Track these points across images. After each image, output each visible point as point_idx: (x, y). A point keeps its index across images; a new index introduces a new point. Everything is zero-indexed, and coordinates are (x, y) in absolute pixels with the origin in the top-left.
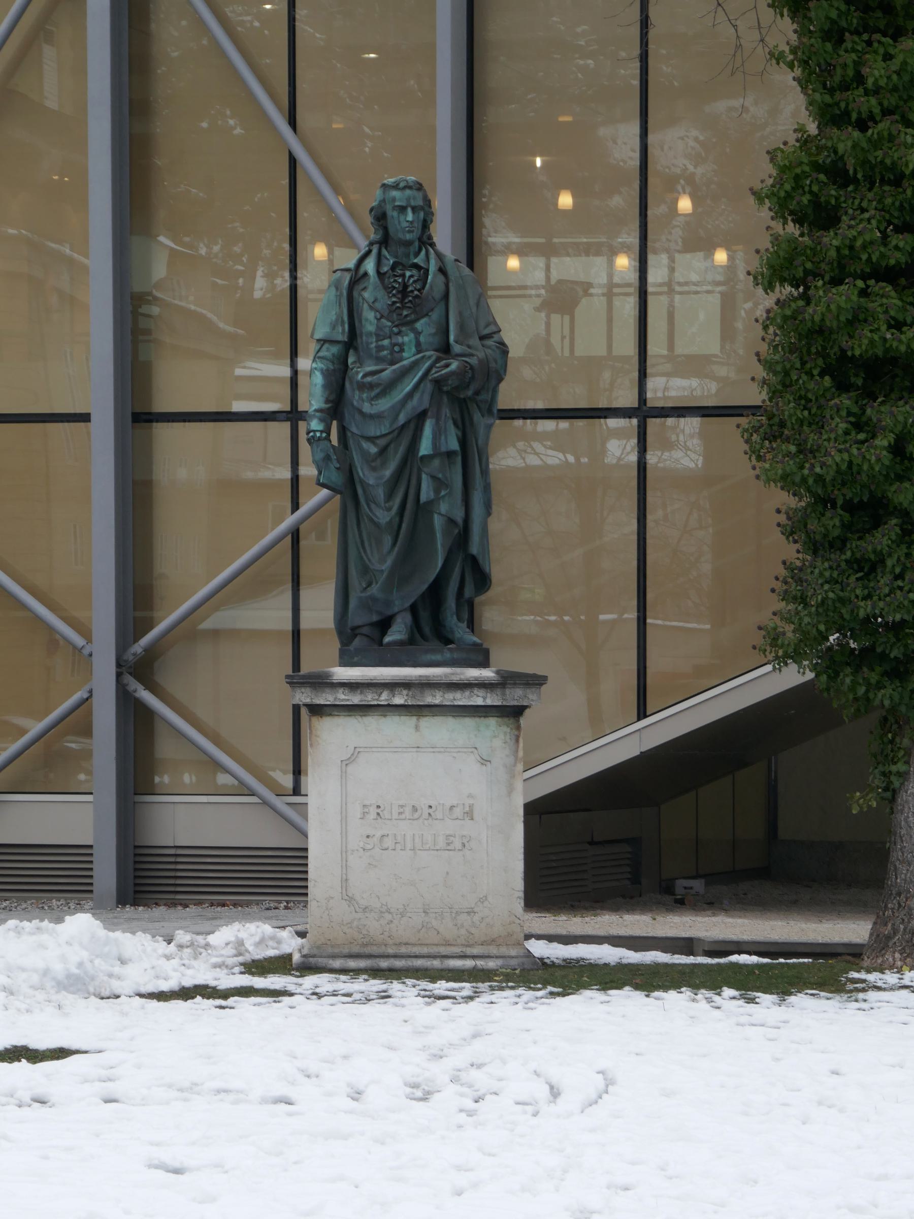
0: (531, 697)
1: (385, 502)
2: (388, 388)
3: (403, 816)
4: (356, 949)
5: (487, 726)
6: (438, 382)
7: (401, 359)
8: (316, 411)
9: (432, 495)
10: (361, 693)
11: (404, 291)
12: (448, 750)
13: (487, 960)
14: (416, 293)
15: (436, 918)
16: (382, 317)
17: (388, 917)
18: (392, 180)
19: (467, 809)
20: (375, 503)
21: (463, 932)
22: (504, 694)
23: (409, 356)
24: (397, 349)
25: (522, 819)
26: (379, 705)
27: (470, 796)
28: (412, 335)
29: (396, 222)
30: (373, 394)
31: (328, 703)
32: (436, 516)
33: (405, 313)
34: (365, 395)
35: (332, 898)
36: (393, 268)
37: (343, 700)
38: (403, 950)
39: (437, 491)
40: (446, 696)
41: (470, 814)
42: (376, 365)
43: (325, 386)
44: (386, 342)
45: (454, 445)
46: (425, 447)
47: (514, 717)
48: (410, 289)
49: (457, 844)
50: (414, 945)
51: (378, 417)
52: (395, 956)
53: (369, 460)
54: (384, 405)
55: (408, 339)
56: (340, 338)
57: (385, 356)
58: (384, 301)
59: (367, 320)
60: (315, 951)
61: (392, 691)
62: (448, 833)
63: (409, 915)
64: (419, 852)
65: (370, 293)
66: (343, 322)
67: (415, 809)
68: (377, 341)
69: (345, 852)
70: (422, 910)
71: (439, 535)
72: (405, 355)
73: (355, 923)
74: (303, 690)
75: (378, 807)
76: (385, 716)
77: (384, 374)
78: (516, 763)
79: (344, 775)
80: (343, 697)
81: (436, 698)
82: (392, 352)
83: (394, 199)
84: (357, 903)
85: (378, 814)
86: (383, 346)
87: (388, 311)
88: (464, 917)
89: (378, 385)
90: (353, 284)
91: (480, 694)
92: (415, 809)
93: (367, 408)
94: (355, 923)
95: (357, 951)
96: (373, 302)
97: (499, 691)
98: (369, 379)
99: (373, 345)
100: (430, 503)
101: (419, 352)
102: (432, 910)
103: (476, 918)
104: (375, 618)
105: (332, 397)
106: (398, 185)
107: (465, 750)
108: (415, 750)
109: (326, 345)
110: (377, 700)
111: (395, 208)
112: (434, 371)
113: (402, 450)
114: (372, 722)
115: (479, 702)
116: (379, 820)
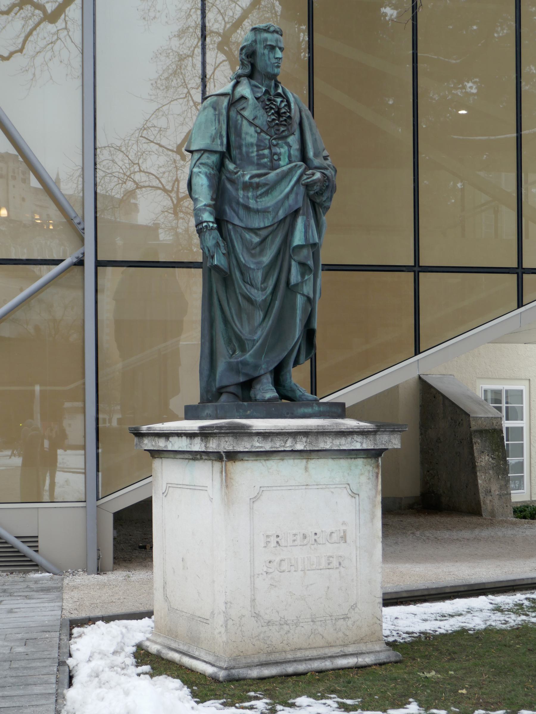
0: (394, 441)
1: (262, 283)
2: (271, 188)
3: (296, 543)
4: (263, 658)
5: (356, 466)
6: (307, 186)
7: (279, 167)
8: (205, 205)
10: (271, 441)
11: (278, 114)
12: (328, 486)
13: (364, 656)
15: (321, 626)
17: (286, 628)
18: (264, 25)
19: (342, 534)
20: (252, 285)
21: (341, 635)
22: (375, 440)
23: (284, 165)
24: (276, 157)
25: (381, 540)
26: (284, 451)
27: (344, 523)
28: (286, 148)
29: (267, 58)
30: (259, 193)
31: (247, 450)
32: (299, 296)
33: (282, 129)
34: (250, 194)
35: (244, 616)
37: (258, 447)
38: (299, 655)
39: (303, 275)
40: (334, 442)
41: (344, 538)
42: (258, 169)
43: (210, 186)
44: (266, 152)
46: (298, 239)
47: (375, 458)
49: (335, 563)
50: (306, 649)
51: (264, 211)
52: (295, 661)
53: (249, 248)
54: (268, 202)
55: (283, 150)
56: (219, 149)
57: (266, 163)
58: (263, 119)
59: (247, 133)
60: (233, 663)
61: (294, 438)
62: (328, 554)
63: (301, 624)
64: (308, 572)
66: (221, 136)
67: (305, 537)
68: (257, 151)
69: (253, 576)
70: (310, 620)
71: (299, 312)
72: (282, 163)
73: (262, 636)
74: (227, 439)
75: (278, 536)
76: (283, 460)
78: (376, 494)
79: (251, 508)
80: (258, 444)
81: (327, 444)
83: (266, 40)
84: (263, 619)
85: (277, 542)
86: (264, 155)
87: (267, 127)
88: (341, 622)
89: (265, 185)
90: (232, 104)
91: (359, 440)
92: (305, 537)
93: (252, 204)
94: (262, 636)
95: (264, 659)
96: (253, 119)
97: (371, 437)
98: (257, 180)
99: (255, 154)
100: (297, 285)
101: (290, 162)
102: (318, 619)
103: (350, 623)
104: (242, 379)
106: (269, 28)
108: (304, 487)
110: (284, 446)
112: (305, 177)
113: (278, 241)
114: (273, 464)
115: (358, 446)
116: (278, 548)
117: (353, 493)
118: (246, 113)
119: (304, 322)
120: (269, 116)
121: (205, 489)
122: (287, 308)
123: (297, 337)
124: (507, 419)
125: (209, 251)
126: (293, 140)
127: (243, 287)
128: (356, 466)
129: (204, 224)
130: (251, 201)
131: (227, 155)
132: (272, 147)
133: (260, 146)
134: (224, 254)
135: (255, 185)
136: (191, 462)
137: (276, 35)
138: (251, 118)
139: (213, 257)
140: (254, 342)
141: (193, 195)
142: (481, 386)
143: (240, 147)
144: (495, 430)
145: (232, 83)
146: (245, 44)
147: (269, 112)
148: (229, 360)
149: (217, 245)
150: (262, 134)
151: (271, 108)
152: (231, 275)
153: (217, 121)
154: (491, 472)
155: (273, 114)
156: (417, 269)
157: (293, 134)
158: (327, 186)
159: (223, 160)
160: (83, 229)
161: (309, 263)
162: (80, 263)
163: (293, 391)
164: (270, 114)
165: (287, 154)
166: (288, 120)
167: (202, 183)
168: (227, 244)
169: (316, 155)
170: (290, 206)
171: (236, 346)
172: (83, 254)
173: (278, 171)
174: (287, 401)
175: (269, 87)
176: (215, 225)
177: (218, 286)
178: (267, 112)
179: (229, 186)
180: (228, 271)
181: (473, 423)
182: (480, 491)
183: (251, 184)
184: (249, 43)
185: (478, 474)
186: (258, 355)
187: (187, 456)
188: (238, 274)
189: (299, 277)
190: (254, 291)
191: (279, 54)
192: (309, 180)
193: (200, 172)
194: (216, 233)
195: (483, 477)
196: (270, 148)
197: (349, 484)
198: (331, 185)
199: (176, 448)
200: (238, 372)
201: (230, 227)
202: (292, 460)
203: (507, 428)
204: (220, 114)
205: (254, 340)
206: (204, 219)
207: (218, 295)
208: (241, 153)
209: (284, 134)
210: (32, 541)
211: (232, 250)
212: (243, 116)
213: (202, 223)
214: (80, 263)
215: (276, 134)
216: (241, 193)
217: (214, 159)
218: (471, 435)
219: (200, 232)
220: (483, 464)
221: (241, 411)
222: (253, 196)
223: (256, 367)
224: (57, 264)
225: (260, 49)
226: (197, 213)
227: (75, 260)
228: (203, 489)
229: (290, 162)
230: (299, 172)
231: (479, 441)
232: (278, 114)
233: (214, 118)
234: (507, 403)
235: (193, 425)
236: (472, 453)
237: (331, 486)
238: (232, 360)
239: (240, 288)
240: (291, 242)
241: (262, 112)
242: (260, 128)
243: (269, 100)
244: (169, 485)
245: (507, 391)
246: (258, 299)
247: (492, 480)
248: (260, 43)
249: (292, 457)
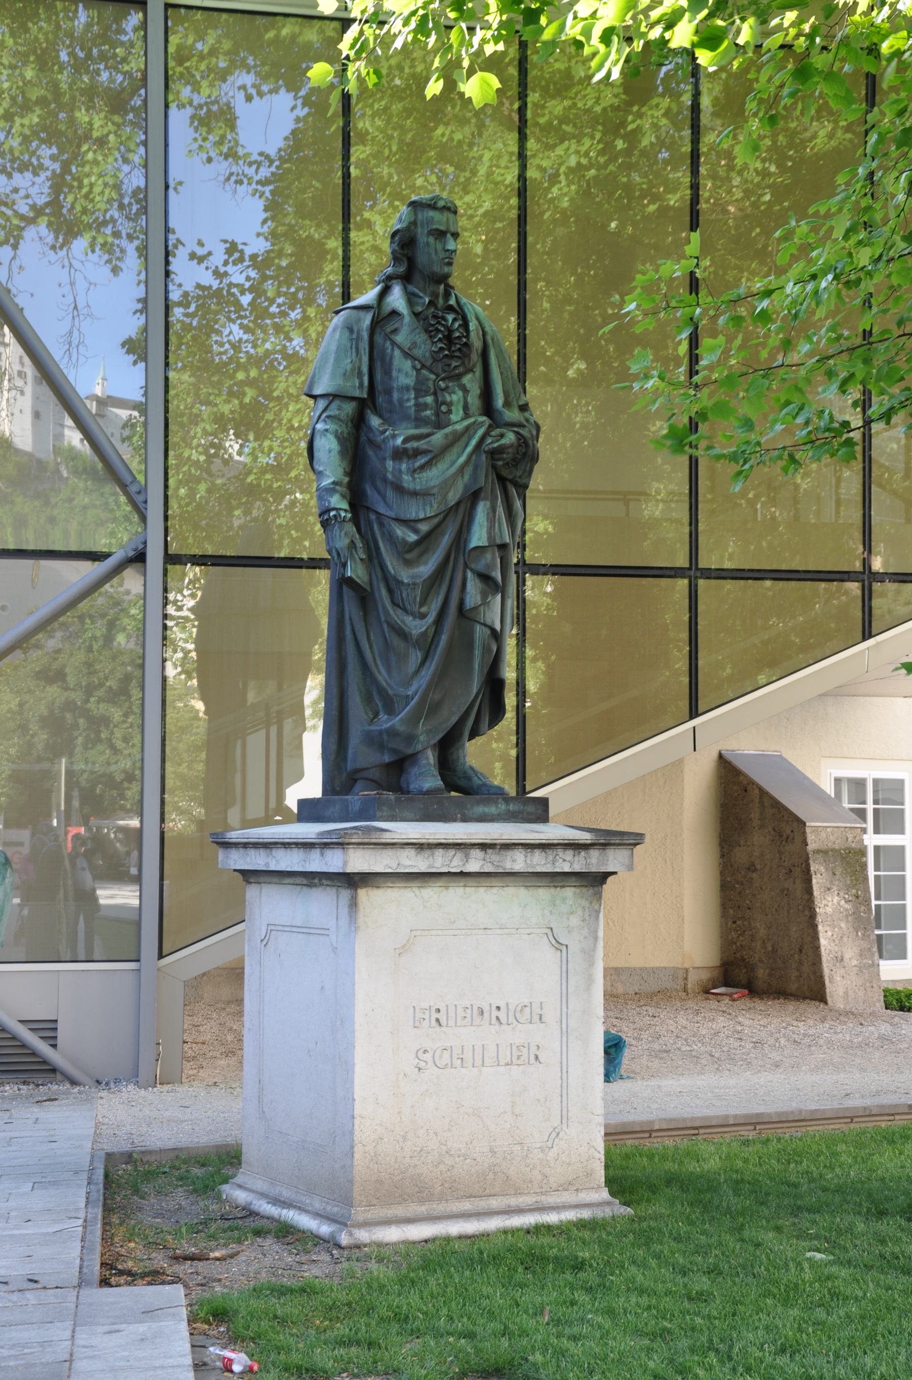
2: (435, 457)
6: (493, 454)
9: (479, 600)
11: (449, 338)
20: (405, 610)
24: (444, 408)
28: (460, 394)
29: (432, 251)
30: (418, 464)
32: (478, 627)
33: (454, 364)
34: (404, 466)
39: (484, 595)
42: (416, 427)
43: (343, 453)
44: (429, 399)
46: (478, 537)
48: (457, 334)
54: (433, 476)
56: (357, 393)
58: (424, 347)
59: (399, 371)
65: (406, 333)
66: (360, 374)
68: (416, 398)
76: (447, 887)
77: (433, 438)
81: (518, 862)
82: (438, 413)
83: (431, 220)
89: (426, 452)
98: (414, 444)
99: (412, 402)
100: (475, 609)
104: (387, 758)
108: (481, 932)
109: (337, 403)
111: (432, 232)
112: (489, 440)
113: (446, 540)
114: (431, 893)
118: (399, 338)
119: (486, 671)
120: (433, 343)
121: (327, 932)
122: (463, 643)
123: (475, 691)
124: (877, 831)
125: (339, 554)
126: (472, 381)
127: (392, 612)
129: (332, 513)
130: (405, 477)
131: (370, 404)
132: (439, 393)
133: (420, 389)
134: (361, 560)
135: (411, 453)
136: (305, 888)
137: (446, 214)
138: (406, 345)
139: (344, 565)
140: (408, 699)
141: (316, 467)
142: (829, 771)
143: (388, 392)
144: (849, 851)
145: (378, 288)
146: (398, 227)
147: (435, 337)
148: (367, 728)
149: (352, 544)
150: (424, 372)
151: (438, 330)
152: (372, 593)
154: (843, 925)
155: (440, 340)
156: (694, 572)
157: (472, 371)
158: (525, 455)
159: (360, 414)
160: (146, 502)
161: (493, 574)
162: (139, 558)
163: (469, 778)
165: (462, 403)
166: (464, 349)
167: (328, 447)
168: (368, 544)
169: (507, 404)
171: (380, 704)
172: (145, 543)
174: (461, 791)
175: (435, 295)
176: (349, 515)
177: (352, 609)
178: (431, 337)
179: (370, 452)
180: (368, 589)
181: (810, 837)
182: (824, 959)
183: (405, 451)
184: (405, 225)
185: (820, 928)
186: (414, 719)
187: (299, 880)
188: (384, 592)
189: (479, 598)
190: (409, 619)
191: (451, 245)
192: (495, 445)
193: (326, 430)
194: (351, 528)
195: (830, 933)
196: (435, 394)
198: (530, 452)
199: (282, 867)
200: (382, 747)
201: (373, 517)
203: (877, 849)
204: (359, 339)
205: (407, 696)
206: (332, 505)
207: (352, 624)
208: (390, 402)
210: (48, 1029)
211: (374, 554)
212: (394, 343)
213: (329, 510)
215: (445, 371)
216: (390, 464)
217: (349, 408)
218: (807, 859)
219: (325, 524)
220: (829, 910)
221: (385, 808)
222: (408, 469)
223: (410, 739)
225: (422, 237)
226: (323, 493)
227: (131, 554)
228: (322, 932)
229: (467, 415)
230: (480, 432)
231: (822, 869)
232: (449, 338)
234: (876, 802)
235: (310, 830)
236: (809, 891)
238: (373, 728)
239: (387, 613)
240: (466, 542)
241: (424, 336)
242: (420, 362)
243: (435, 317)
244: (270, 927)
245: (876, 782)
246: (414, 632)
247: (845, 939)
248: (422, 227)
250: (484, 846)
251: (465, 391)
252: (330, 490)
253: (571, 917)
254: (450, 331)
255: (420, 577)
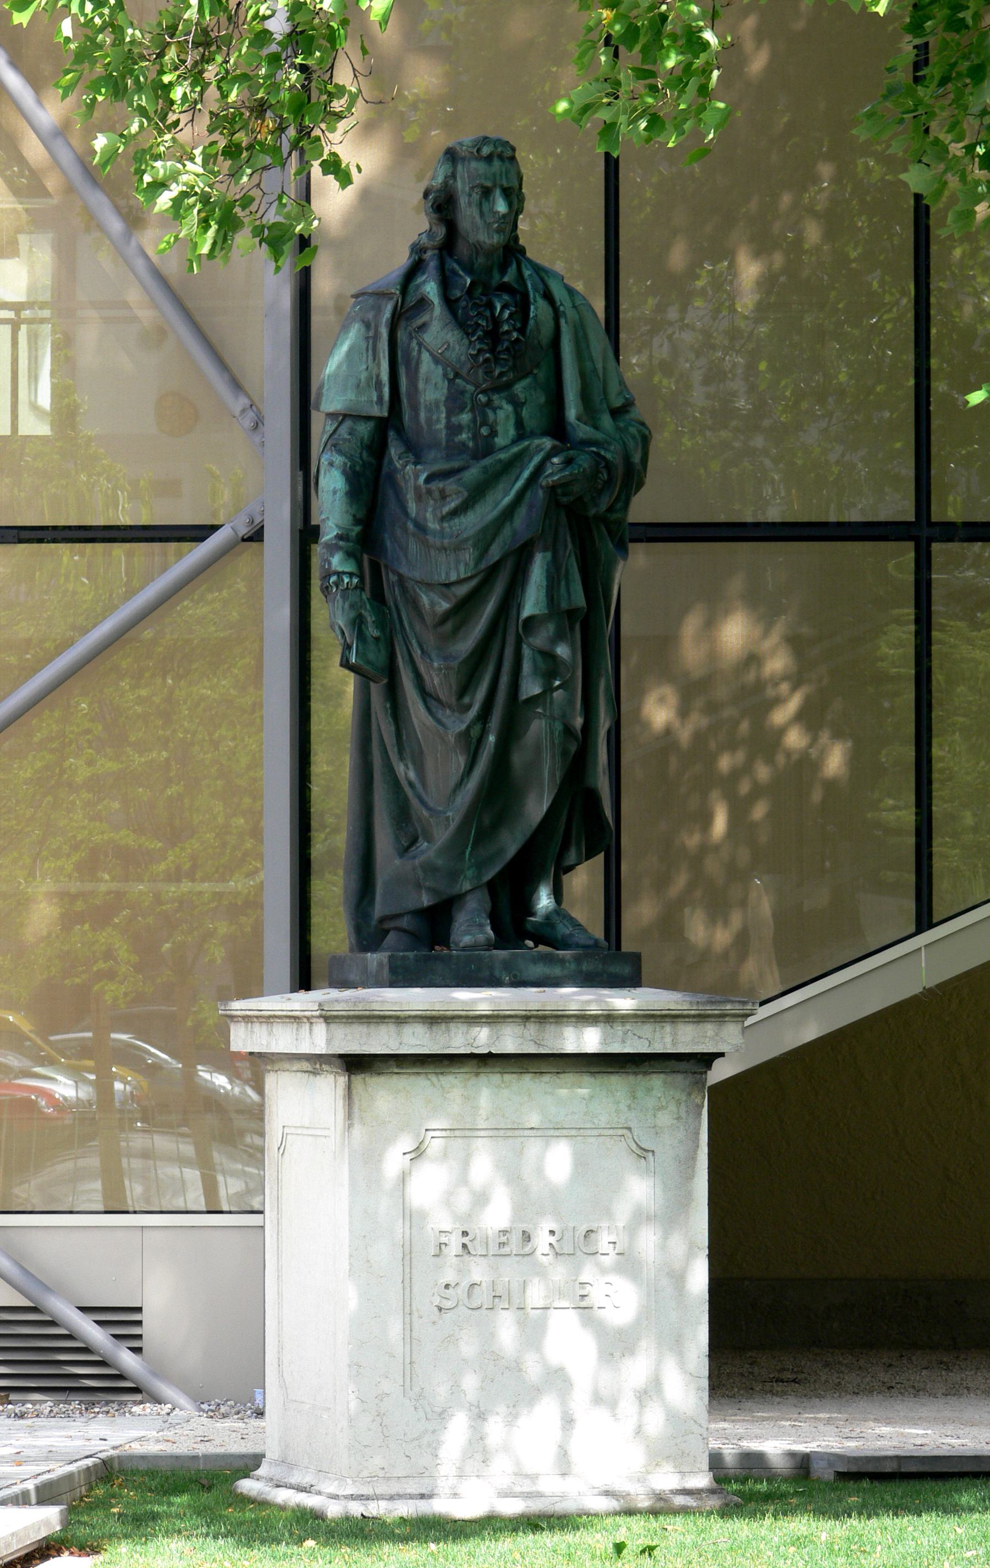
3: (506, 1250)
14: (515, 335)
16: (457, 375)
28: (509, 408)
36: (470, 291)
45: (579, 599)
46: (532, 602)
48: (506, 328)
56: (376, 411)
66: (379, 385)
76: (477, 1074)
104: (426, 900)
105: (360, 515)
107: (611, 1132)
109: (348, 424)
113: (490, 607)
114: (453, 1084)
116: (466, 1257)
117: (641, 1148)
128: (649, 1090)
153: (370, 352)
162: (257, 536)
164: (473, 339)
165: (512, 421)
169: (589, 412)
170: (515, 533)
173: (487, 461)
197: (629, 1129)
202: (499, 1076)
209: (505, 379)
214: (257, 536)
217: (364, 429)
224: (202, 539)
230: (536, 460)
233: (364, 346)
237: (589, 1132)
240: (519, 608)
249: (497, 1069)
250: (526, 1018)
251: (517, 405)
252: (192, 600)
253: (659, 1114)
254: (496, 322)
255: (455, 658)
